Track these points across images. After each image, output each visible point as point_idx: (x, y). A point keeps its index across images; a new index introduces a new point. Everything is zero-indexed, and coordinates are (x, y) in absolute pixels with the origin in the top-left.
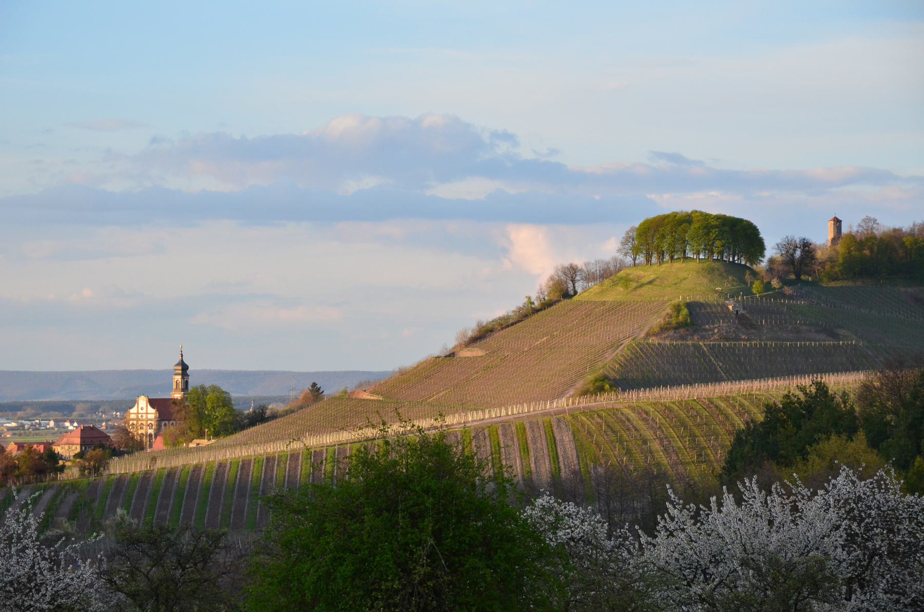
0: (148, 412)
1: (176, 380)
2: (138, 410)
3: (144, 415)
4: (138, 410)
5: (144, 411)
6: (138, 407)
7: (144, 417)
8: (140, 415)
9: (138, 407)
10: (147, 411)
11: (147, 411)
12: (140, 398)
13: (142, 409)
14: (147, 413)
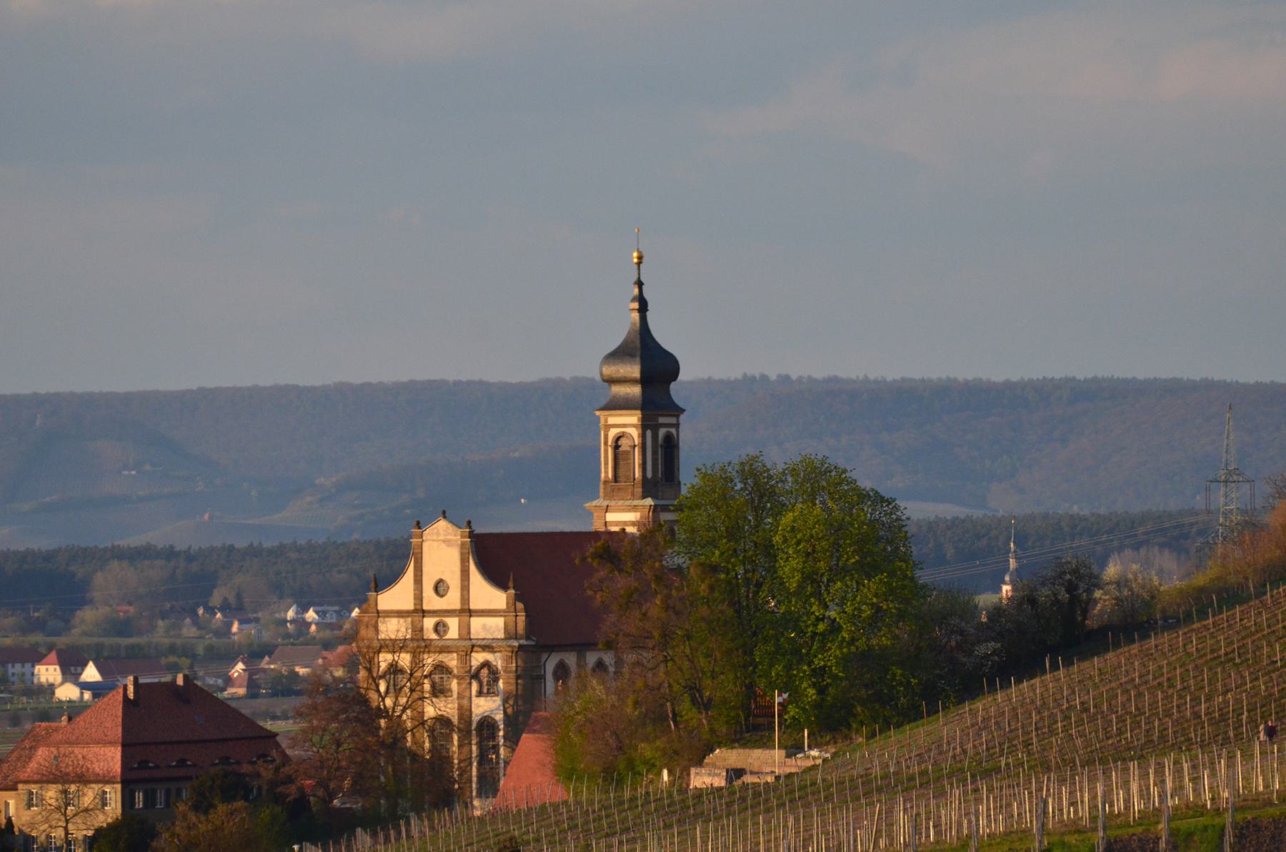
2: (419, 597)
3: (453, 623)
4: (419, 597)
5: (452, 600)
6: (418, 580)
7: (453, 632)
8: (429, 623)
9: (418, 580)
10: (465, 597)
11: (465, 597)
12: (428, 533)
13: (440, 588)
14: (466, 612)
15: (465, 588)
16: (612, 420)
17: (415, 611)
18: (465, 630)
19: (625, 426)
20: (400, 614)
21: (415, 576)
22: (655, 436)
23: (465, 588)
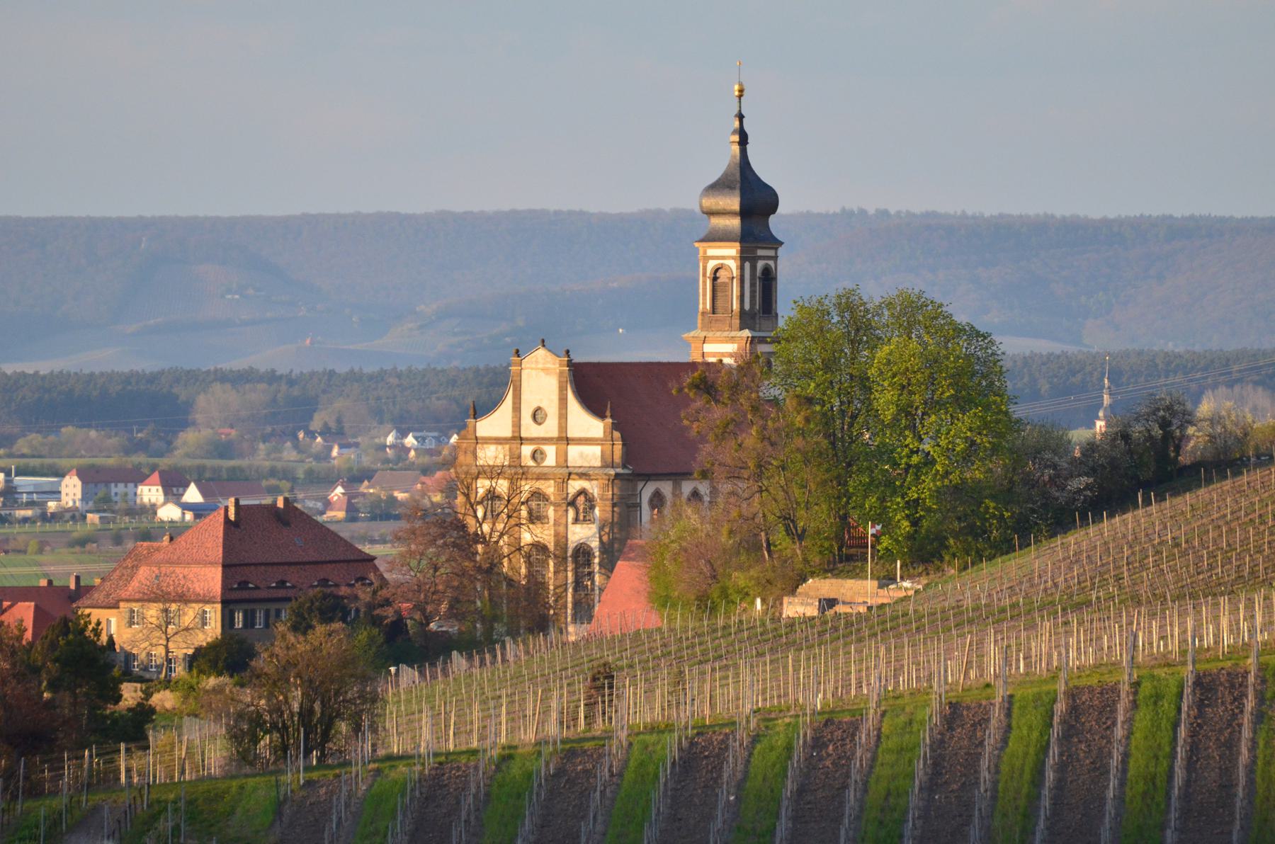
0: (571, 433)
1: (712, 264)
2: (517, 425)
3: (551, 451)
4: (517, 425)
5: (550, 428)
6: (517, 408)
7: (550, 460)
8: (527, 450)
9: (517, 408)
10: (563, 425)
11: (563, 425)
13: (538, 416)
14: (564, 440)
16: (711, 252)
17: (513, 438)
18: (563, 458)
19: (723, 258)
20: (498, 441)
21: (514, 403)
22: (753, 268)
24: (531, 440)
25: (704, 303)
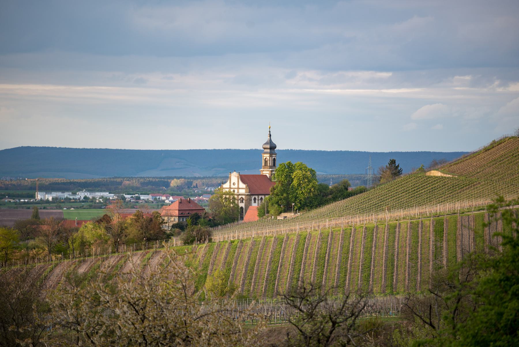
0: (240, 187)
2: (230, 185)
4: (230, 185)
5: (236, 186)
10: (238, 186)
11: (238, 186)
14: (238, 188)
15: (238, 184)
16: (264, 155)
17: (238, 188)
22: (272, 158)
23: (238, 184)
24: (233, 188)
25: (270, 163)
